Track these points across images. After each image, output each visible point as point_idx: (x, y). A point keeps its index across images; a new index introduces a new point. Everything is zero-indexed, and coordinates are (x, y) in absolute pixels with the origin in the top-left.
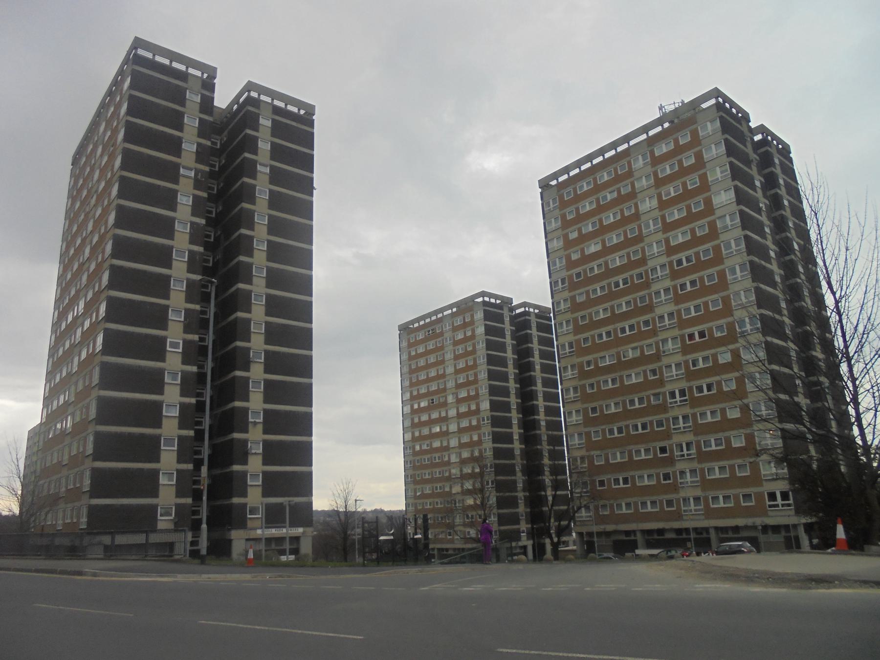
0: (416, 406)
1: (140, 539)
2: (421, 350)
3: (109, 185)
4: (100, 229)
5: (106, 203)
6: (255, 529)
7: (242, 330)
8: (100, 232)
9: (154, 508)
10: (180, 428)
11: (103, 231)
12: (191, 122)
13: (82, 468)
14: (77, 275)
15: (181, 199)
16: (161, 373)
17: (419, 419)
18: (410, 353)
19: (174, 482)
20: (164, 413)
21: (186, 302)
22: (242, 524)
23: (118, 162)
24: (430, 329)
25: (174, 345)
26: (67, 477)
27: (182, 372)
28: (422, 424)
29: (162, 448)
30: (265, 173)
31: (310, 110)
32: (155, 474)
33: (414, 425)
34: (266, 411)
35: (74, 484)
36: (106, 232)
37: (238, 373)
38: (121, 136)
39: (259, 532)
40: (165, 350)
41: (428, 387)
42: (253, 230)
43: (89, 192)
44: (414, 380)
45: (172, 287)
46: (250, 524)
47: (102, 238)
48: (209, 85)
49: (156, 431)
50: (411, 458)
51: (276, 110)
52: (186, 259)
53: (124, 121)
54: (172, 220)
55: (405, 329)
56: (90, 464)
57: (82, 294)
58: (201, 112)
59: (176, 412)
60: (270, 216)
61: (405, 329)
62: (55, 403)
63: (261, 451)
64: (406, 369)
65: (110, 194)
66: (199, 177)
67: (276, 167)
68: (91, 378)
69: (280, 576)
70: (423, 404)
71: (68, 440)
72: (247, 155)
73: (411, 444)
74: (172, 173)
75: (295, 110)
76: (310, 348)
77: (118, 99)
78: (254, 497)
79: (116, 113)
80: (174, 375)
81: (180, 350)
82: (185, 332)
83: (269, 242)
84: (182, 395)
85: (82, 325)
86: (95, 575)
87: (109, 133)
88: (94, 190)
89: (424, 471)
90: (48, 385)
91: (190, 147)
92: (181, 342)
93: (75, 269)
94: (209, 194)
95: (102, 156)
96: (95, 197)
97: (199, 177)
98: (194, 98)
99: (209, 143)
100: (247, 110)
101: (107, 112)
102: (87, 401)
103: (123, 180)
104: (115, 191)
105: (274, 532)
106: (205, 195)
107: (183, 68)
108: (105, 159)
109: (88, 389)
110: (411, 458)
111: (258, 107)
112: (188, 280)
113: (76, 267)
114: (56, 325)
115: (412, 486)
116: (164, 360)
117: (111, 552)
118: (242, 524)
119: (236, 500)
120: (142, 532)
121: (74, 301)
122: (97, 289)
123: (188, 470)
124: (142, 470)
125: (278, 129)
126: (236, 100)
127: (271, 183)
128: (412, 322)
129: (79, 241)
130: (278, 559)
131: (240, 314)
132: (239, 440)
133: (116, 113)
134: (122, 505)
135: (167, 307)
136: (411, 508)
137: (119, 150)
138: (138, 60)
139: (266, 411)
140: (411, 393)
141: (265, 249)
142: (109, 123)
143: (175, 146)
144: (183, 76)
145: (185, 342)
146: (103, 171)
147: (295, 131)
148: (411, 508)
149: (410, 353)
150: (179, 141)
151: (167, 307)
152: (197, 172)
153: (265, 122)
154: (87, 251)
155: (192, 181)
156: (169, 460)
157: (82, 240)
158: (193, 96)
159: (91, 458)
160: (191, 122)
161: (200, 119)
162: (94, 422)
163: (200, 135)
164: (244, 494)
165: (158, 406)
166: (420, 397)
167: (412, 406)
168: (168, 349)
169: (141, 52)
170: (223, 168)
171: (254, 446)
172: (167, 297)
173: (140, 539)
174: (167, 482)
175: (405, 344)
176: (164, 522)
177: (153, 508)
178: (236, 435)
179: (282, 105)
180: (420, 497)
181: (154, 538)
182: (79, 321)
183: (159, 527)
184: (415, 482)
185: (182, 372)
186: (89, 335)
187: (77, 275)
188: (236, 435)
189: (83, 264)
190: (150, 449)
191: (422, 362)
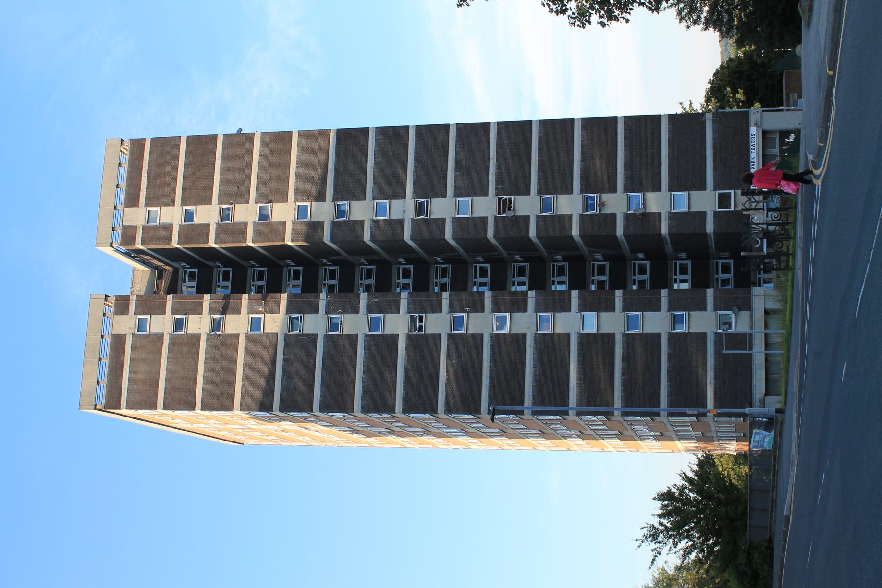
15: (591, 327)
27: (536, 311)
32: (497, 339)
94: (614, 286)
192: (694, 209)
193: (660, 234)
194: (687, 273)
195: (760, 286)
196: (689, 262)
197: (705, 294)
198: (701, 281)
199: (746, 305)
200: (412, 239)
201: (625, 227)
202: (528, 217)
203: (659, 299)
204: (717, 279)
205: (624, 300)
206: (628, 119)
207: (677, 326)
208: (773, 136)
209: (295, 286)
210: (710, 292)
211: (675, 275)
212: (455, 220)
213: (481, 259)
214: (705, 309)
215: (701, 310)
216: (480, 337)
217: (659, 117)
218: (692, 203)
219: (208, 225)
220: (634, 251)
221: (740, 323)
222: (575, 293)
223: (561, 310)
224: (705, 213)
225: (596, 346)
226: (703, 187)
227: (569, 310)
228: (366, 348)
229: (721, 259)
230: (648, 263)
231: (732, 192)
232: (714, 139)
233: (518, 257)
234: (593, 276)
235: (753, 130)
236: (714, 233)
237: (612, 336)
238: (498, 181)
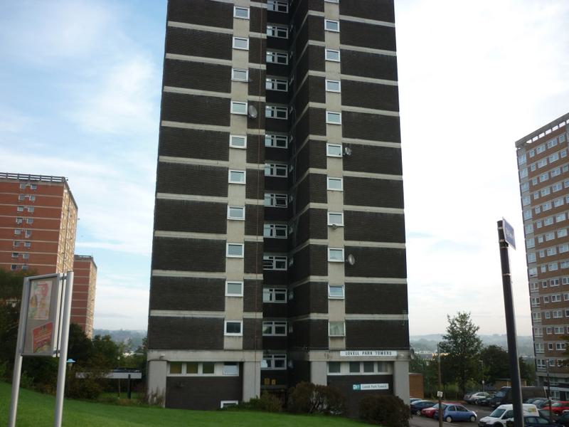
0: (541, 240)
6: (339, 350)
15: (234, 109)
17: (543, 224)
29: (227, 255)
39: (343, 354)
41: (550, 174)
46: (331, 345)
55: (522, 145)
61: (522, 145)
76: (400, 172)
92: (246, 138)
94: (265, 273)
115: (539, 311)
116: (226, 159)
118: (322, 344)
134: (184, 318)
135: (230, 68)
164: (324, 310)
165: (223, 173)
174: (234, 294)
190: (214, 257)
192: (330, 304)
193: (309, 275)
194: (276, 366)
195: (264, 357)
196: (286, 335)
197: (258, 311)
198: (269, 311)
199: (247, 347)
201: (315, 246)
202: (326, 168)
203: (254, 272)
204: (272, 323)
206: (405, 287)
208: (389, 369)
209: (270, 329)
211: (276, 290)
212: (326, 322)
213: (291, 232)
214: (245, 310)
215: (244, 307)
217: (405, 276)
218: (335, 302)
220: (296, 291)
221: (233, 340)
222: (263, 67)
224: (326, 275)
226: (348, 311)
227: (245, 310)
229: (289, 321)
230: (285, 301)
233: (292, 168)
234: (277, 166)
235: (394, 353)
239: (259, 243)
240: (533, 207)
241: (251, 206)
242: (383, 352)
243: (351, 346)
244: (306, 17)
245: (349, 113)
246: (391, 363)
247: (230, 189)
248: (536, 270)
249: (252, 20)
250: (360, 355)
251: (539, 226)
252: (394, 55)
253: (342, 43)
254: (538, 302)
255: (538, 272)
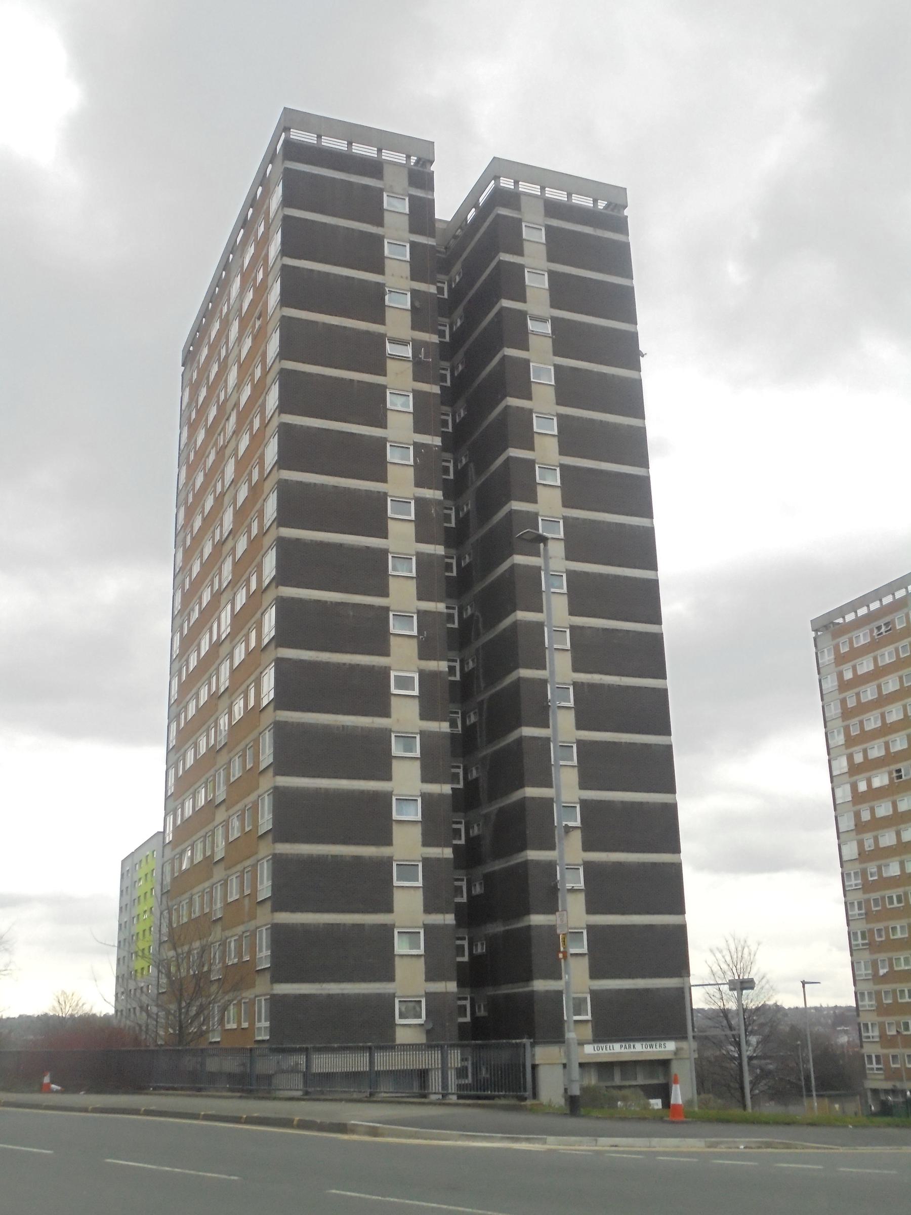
1: (357, 1062)
2: (866, 666)
3: (260, 390)
4: (250, 474)
5: (257, 424)
7: (527, 646)
8: (250, 480)
9: (386, 1002)
10: (425, 844)
11: (255, 477)
12: (397, 253)
13: (252, 925)
14: (211, 565)
15: (392, 402)
16: (384, 736)
18: (840, 675)
19: (421, 951)
20: (395, 816)
21: (420, 598)
22: (555, 1033)
23: (273, 346)
24: (881, 623)
25: (404, 683)
26: (224, 943)
27: (422, 733)
28: (878, 824)
29: (396, 883)
30: (545, 335)
31: (617, 200)
32: (385, 934)
33: (860, 827)
34: (585, 805)
35: (240, 954)
36: (263, 479)
37: (527, 731)
38: (274, 295)
40: (388, 695)
42: (531, 448)
43: (221, 408)
44: (855, 732)
45: (391, 572)
46: (571, 1035)
47: (256, 491)
48: (421, 178)
49: (384, 851)
50: (860, 896)
51: (553, 209)
52: (413, 517)
53: (278, 267)
54: (380, 445)
56: (266, 918)
57: (224, 598)
58: (412, 231)
59: (415, 813)
60: (560, 417)
61: (827, 627)
62: (189, 805)
63: (581, 885)
64: (835, 710)
65: (263, 407)
66: (422, 356)
67: (563, 320)
68: (256, 756)
69: (769, 1145)
70: (880, 780)
71: (219, 873)
72: (506, 303)
73: (857, 867)
74: (370, 353)
75: (588, 202)
77: (261, 229)
78: (576, 980)
79: (260, 257)
80: (406, 739)
81: (416, 692)
82: (423, 656)
83: (563, 467)
84: (425, 780)
85: (231, 656)
86: (374, 1132)
87: (250, 295)
88: (230, 404)
89: (891, 924)
90: (172, 772)
91: (399, 303)
92: (416, 676)
93: (206, 556)
95: (239, 340)
96: (233, 419)
97: (422, 356)
98: (396, 206)
99: (433, 289)
100: (495, 219)
101: (242, 257)
102: (253, 797)
103: (286, 378)
104: (273, 398)
105: (616, 1050)
106: (436, 389)
107: (370, 152)
108: (248, 343)
109: (252, 775)
110: (860, 896)
111: (518, 208)
112: (419, 555)
113: (208, 550)
114: (178, 659)
115: (866, 955)
116: (386, 714)
117: (318, 1086)
118: (555, 1033)
119: (540, 985)
120: (363, 1049)
121: (210, 613)
122: (253, 586)
123: (446, 926)
124: (360, 927)
125: (559, 246)
126: (471, 200)
127: (555, 354)
128: (842, 611)
129: (209, 503)
130: (646, 1107)
131: (522, 615)
132: (537, 863)
133: (260, 257)
134: (330, 996)
136: (867, 1002)
137: (274, 323)
138: (293, 150)
139: (585, 805)
140: (850, 758)
141: (558, 483)
142: (247, 277)
143: (372, 303)
144: (374, 168)
145: (424, 676)
146: (244, 368)
147: (592, 246)
148: (867, 1002)
149: (840, 675)
150: (379, 292)
151: (387, 609)
152: (417, 346)
153: (534, 236)
154: (228, 518)
155: (409, 366)
156: (409, 906)
157: (216, 499)
158: (395, 202)
159: (268, 905)
160: (397, 253)
161: (413, 245)
162: (270, 837)
163: (416, 275)
164: (532, 498)
165: (382, 802)
166: (870, 766)
167: (854, 787)
168: (394, 690)
169: (296, 135)
170: (458, 338)
171: (569, 875)
172: (385, 593)
173: (357, 1062)
175: (828, 658)
176: (408, 1030)
177: (386, 1002)
178: (533, 855)
179: (561, 196)
180: (885, 979)
181: (385, 1061)
182: (224, 650)
183: (398, 1041)
184: (873, 947)
185: (422, 733)
186: (245, 675)
187: (211, 565)
188: (533, 855)
189: (223, 543)
190: (371, 886)
191: (869, 693)
200: (515, 624)
205: (438, 860)
206: (682, 930)
207: (405, 938)
210: (452, 986)
216: (386, 653)
219: (525, 301)
223: (424, 768)
225: (374, 819)
228: (368, 493)
231: (589, 1017)
232: (658, 989)
235: (671, 1046)
236: (533, 991)
237: (391, 978)
238: (592, 686)
239: (446, 859)
240: (849, 751)
241: (430, 795)
242: (654, 1043)
243: (602, 1034)
244: (493, 264)
245: (582, 628)
246: (665, 1064)
247: (396, 830)
248: (854, 845)
249: (420, 577)
250: (616, 1050)
251: (859, 758)
252: (653, 578)
253: (565, 505)
254: (863, 938)
255: (842, 708)
